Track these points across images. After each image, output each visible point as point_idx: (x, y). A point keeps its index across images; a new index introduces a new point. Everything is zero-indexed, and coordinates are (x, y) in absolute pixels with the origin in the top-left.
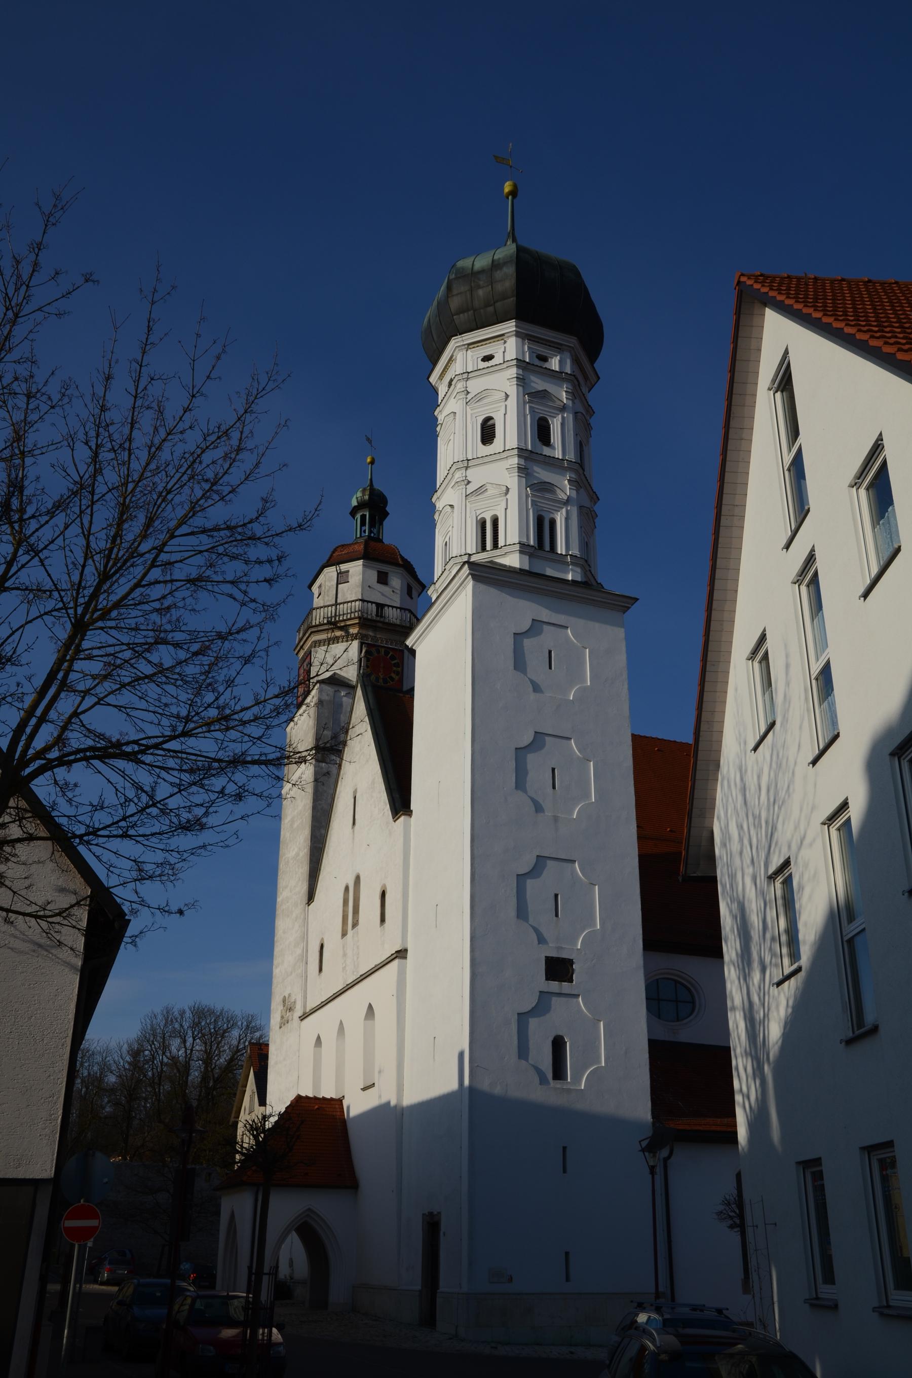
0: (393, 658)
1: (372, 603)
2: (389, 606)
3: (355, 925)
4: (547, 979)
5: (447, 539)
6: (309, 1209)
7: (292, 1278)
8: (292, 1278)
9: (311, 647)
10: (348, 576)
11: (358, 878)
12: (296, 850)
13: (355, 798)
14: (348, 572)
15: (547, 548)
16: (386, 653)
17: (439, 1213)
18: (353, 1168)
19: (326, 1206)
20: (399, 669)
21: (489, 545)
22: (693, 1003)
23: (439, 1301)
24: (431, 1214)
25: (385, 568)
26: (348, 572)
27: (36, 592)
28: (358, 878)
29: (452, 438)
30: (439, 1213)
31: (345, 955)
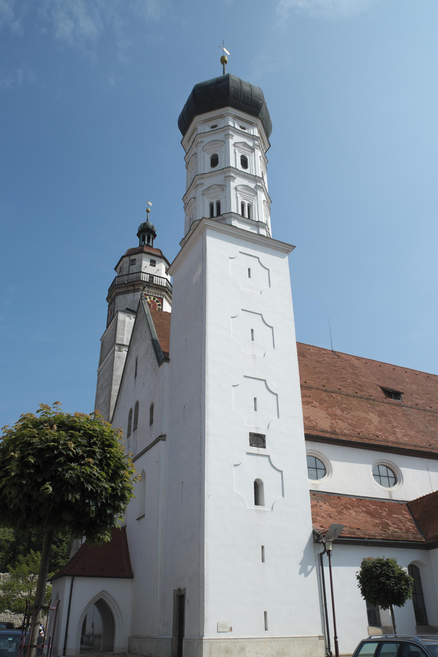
0: (157, 301)
1: (147, 274)
2: (156, 276)
3: (135, 429)
4: (251, 445)
5: (191, 216)
6: (104, 591)
7: (93, 634)
8: (93, 634)
9: (115, 295)
10: (135, 262)
11: (137, 404)
12: (104, 398)
13: (137, 362)
14: (135, 259)
15: (247, 217)
16: (154, 299)
17: (185, 589)
18: (130, 566)
19: (115, 590)
20: (161, 307)
21: (215, 214)
22: (325, 469)
23: (184, 645)
24: (179, 590)
25: (154, 258)
26: (135, 259)
27: (66, 561)
28: (137, 404)
29: (194, 167)
30: (185, 589)
31: (129, 447)
